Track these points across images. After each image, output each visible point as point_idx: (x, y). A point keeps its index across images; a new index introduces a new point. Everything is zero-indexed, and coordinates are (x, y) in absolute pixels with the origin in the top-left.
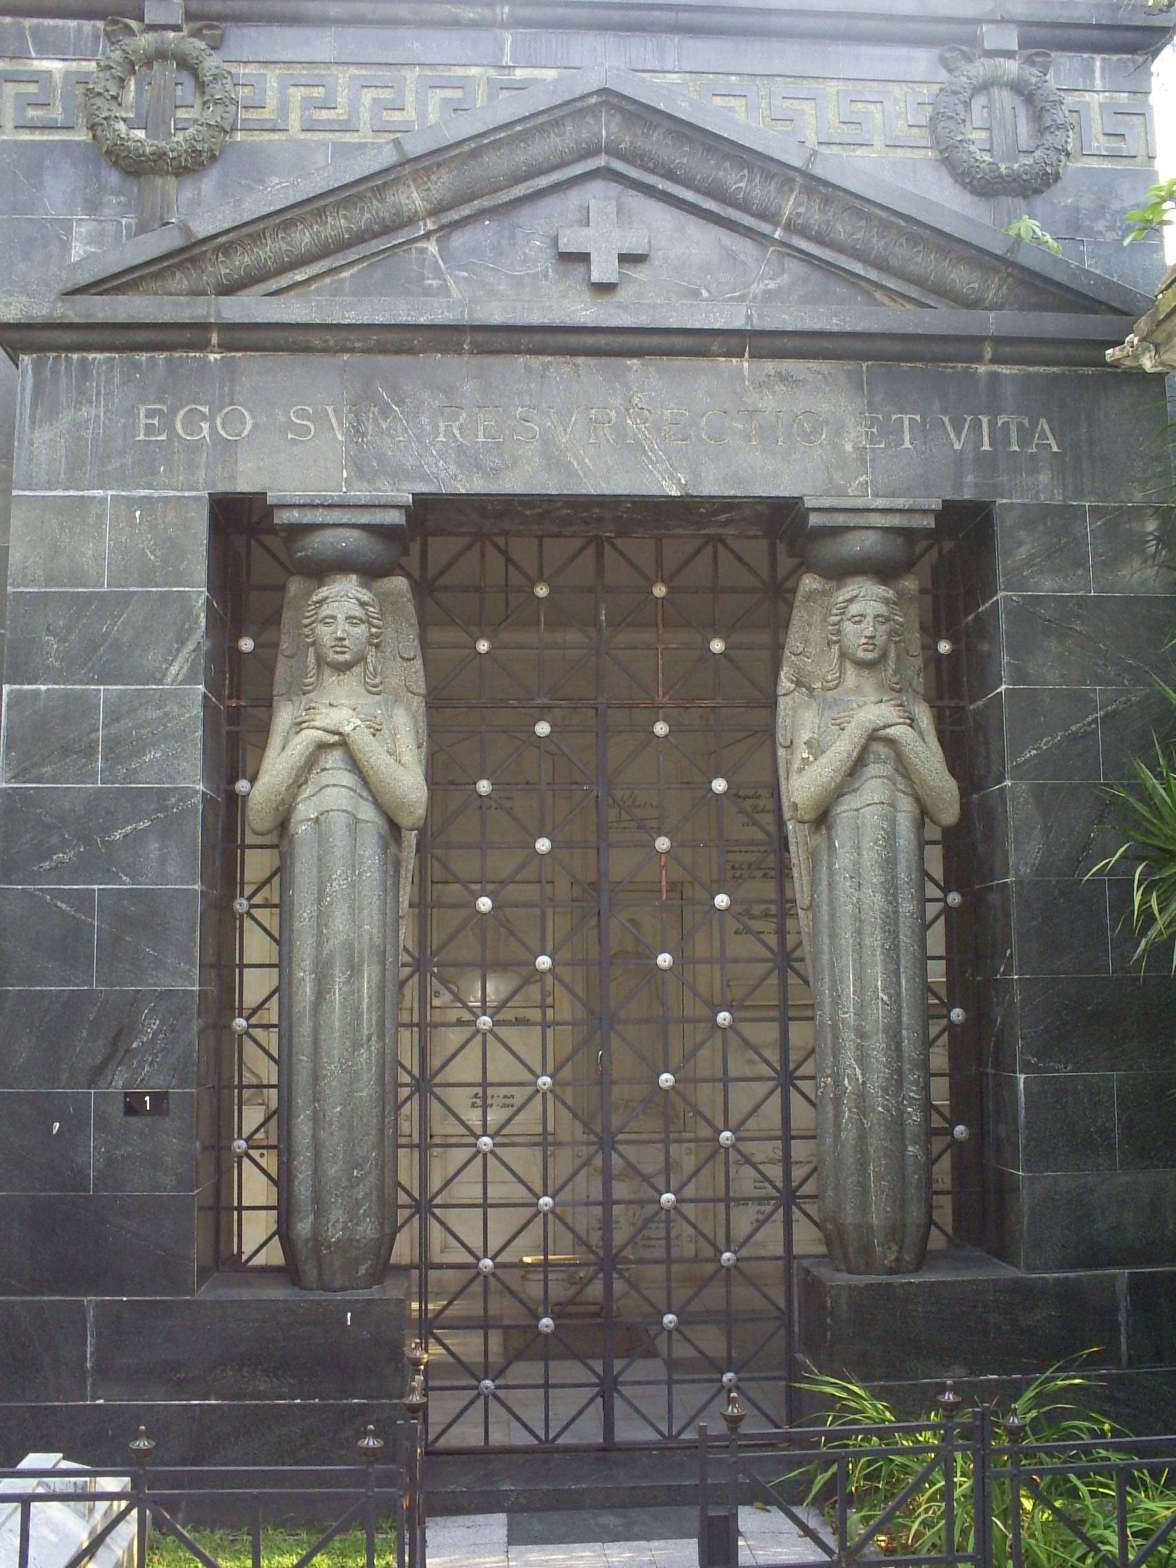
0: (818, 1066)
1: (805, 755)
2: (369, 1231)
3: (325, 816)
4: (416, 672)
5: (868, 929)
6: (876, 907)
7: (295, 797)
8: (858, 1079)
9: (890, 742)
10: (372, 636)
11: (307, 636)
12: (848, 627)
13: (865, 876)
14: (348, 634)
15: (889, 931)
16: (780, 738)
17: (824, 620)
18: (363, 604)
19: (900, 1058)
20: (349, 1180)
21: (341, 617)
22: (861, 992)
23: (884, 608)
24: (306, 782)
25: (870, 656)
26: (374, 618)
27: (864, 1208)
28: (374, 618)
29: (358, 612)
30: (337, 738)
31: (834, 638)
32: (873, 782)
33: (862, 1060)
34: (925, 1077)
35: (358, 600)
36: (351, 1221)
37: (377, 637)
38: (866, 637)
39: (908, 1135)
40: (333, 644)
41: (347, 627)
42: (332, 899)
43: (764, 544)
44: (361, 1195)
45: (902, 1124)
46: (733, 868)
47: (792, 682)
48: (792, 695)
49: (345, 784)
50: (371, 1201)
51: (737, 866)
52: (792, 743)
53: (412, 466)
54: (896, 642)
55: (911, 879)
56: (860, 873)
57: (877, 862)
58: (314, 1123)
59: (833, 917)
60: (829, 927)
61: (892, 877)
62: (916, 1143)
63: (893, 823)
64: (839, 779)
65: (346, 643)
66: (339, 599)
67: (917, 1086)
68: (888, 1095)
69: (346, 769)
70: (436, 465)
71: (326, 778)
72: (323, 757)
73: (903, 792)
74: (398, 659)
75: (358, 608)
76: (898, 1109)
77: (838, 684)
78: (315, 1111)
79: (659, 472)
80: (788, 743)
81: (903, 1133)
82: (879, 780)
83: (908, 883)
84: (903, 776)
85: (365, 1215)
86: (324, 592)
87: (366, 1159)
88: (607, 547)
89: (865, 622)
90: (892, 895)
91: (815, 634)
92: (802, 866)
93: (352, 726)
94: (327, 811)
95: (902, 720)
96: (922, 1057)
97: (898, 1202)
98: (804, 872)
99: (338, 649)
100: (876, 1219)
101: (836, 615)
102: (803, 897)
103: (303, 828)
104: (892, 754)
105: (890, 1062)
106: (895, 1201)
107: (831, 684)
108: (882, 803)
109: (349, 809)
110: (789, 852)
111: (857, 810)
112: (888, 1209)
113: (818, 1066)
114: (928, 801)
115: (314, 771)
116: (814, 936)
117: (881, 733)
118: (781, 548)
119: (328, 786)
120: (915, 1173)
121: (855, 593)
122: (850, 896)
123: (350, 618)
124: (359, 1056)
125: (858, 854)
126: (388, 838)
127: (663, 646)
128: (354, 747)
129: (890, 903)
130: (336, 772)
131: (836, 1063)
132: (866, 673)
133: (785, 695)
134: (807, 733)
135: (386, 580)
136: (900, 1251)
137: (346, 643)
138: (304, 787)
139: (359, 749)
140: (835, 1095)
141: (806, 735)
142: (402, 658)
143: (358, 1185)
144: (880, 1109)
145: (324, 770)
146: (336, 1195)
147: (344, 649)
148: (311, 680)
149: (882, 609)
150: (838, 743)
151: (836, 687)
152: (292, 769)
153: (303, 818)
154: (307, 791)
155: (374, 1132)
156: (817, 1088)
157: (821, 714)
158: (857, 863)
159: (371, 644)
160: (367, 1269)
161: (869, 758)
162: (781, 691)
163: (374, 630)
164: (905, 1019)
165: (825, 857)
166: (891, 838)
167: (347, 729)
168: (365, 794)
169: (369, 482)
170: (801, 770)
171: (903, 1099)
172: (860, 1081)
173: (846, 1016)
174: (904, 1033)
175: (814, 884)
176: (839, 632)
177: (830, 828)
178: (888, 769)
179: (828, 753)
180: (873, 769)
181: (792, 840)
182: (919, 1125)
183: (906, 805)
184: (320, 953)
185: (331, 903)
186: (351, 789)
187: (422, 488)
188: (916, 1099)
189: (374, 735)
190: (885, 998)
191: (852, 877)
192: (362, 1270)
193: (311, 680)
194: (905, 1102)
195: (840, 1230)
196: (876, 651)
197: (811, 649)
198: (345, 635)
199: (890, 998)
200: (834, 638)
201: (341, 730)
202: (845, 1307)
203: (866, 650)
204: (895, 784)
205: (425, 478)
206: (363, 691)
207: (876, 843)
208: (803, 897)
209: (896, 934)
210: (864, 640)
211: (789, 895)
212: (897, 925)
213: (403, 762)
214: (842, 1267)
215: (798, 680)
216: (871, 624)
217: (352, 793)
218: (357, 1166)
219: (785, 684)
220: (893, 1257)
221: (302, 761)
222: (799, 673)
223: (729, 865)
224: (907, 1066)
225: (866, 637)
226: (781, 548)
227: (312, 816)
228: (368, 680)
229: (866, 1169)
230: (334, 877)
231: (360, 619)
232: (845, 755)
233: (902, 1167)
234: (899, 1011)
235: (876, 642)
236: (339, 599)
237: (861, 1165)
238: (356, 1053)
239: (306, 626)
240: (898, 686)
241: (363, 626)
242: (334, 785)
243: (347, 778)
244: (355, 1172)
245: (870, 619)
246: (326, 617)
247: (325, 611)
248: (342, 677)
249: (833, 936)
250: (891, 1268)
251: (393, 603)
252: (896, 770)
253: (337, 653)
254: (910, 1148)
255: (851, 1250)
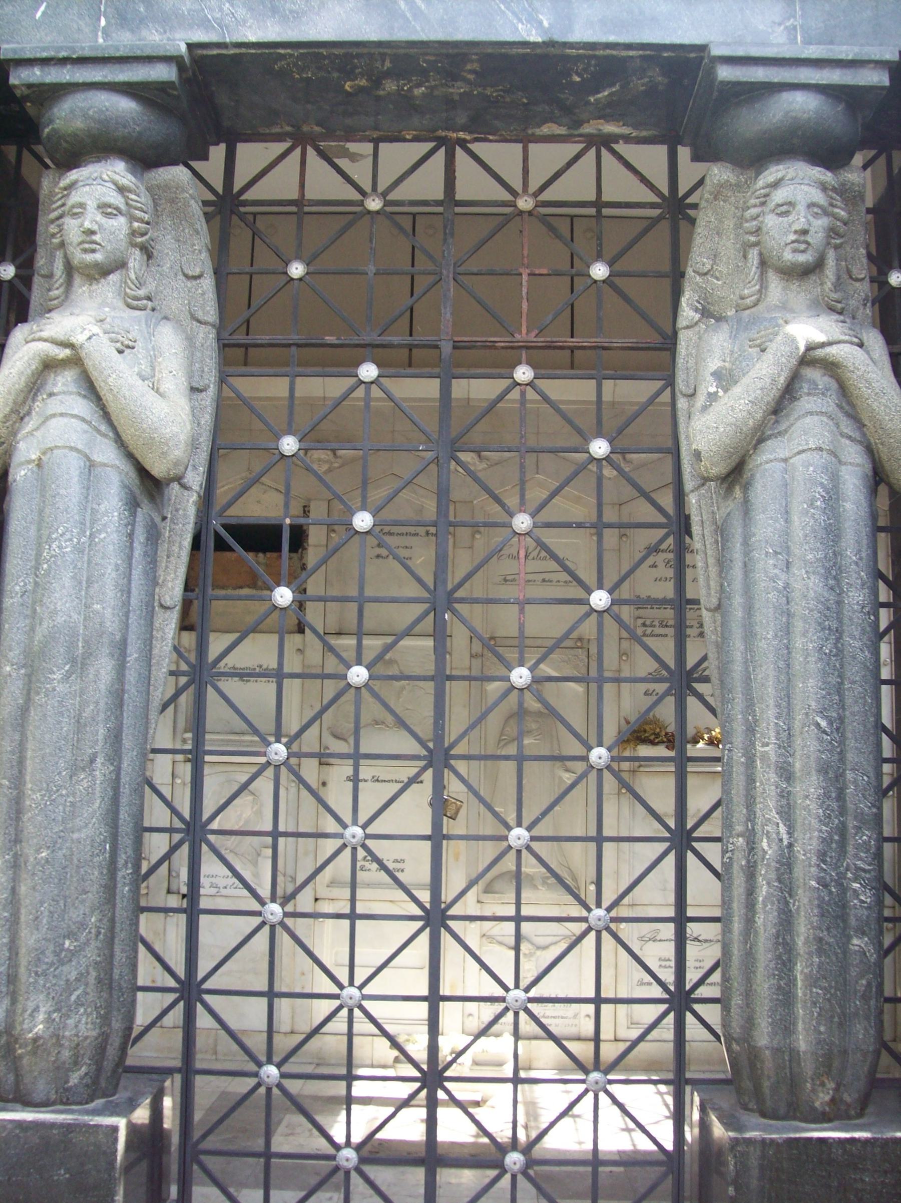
0: (727, 825)
1: (712, 389)
2: (82, 1026)
3: (48, 455)
4: (203, 294)
5: (799, 625)
6: (812, 594)
7: (14, 433)
8: (781, 840)
9: (831, 367)
10: (134, 233)
11: (53, 235)
12: (771, 221)
13: (797, 551)
14: (100, 226)
15: (829, 629)
16: (681, 384)
17: (739, 226)
18: (122, 190)
19: (843, 811)
20: (57, 954)
21: (91, 205)
22: (788, 714)
23: (821, 196)
24: (29, 413)
25: (801, 258)
26: (136, 208)
27: (786, 1026)
28: (136, 208)
29: (117, 200)
30: (67, 352)
31: (753, 239)
32: (808, 420)
33: (787, 813)
34: (877, 840)
35: (115, 183)
36: (58, 1010)
37: (143, 235)
38: (796, 232)
39: (853, 922)
40: (80, 240)
41: (99, 217)
42: (49, 566)
43: (662, 151)
44: (73, 976)
45: (844, 906)
46: (644, 625)
47: (696, 310)
48: (696, 329)
49: (75, 412)
50: (87, 984)
51: (648, 623)
52: (695, 390)
53: (189, 11)
54: (836, 247)
55: (861, 559)
56: (788, 548)
57: (814, 531)
58: (15, 873)
59: (749, 609)
60: (744, 626)
61: (834, 553)
62: (864, 933)
63: (835, 478)
64: (759, 415)
65: (97, 238)
66: (90, 182)
67: (868, 851)
68: (824, 862)
69: (79, 394)
70: (221, 10)
71: (54, 406)
72: (50, 382)
73: (849, 438)
74: (181, 277)
75: (115, 194)
76: (839, 884)
77: (758, 301)
78: (16, 856)
79: (513, 13)
80: (691, 391)
81: (843, 917)
82: (816, 418)
83: (856, 564)
84: (848, 415)
85: (79, 1003)
86: (73, 175)
87: (82, 925)
88: (459, 151)
89: (794, 214)
90: (835, 578)
91: (728, 246)
92: (709, 552)
93: (87, 334)
94: (51, 449)
95: (847, 338)
96: (874, 810)
97: (836, 1019)
98: (711, 561)
99: (87, 246)
100: (803, 1042)
101: (755, 206)
102: (709, 595)
103: (23, 473)
104: (834, 385)
105: (829, 817)
106: (832, 1017)
107: (748, 301)
108: (820, 449)
109: (80, 447)
110: (691, 537)
111: (785, 460)
112: (822, 1029)
113: (727, 825)
114: (884, 453)
115: (40, 398)
116: (722, 647)
117: (820, 353)
118: (684, 153)
119: (54, 416)
120: (862, 977)
121: (780, 175)
122: (773, 579)
123: (104, 208)
124: (78, 782)
125: (786, 521)
126: (137, 492)
127: (528, 271)
128: (89, 364)
129: (832, 589)
130: (67, 397)
131: (751, 817)
132: (795, 286)
133: (687, 327)
134: (716, 361)
135: (161, 170)
136: (837, 1090)
137: (97, 238)
138: (26, 419)
139: (94, 366)
140: (748, 862)
141: (714, 364)
142: (186, 276)
143: (70, 960)
144: (813, 883)
145: (51, 395)
146: (36, 973)
147: (94, 246)
148: (56, 292)
149: (818, 197)
150: (758, 366)
151: (755, 305)
152: (9, 393)
153: (23, 459)
154: (30, 424)
155: (95, 888)
156: (724, 852)
157: (733, 337)
158: (787, 533)
159: (134, 245)
160: (82, 1078)
161: (801, 388)
162: (681, 322)
163: (136, 225)
164: (851, 756)
165: (740, 530)
166: (833, 497)
167: (79, 338)
168: (103, 428)
169: (132, 31)
170: (705, 408)
171: (847, 870)
172: (785, 842)
173: (766, 749)
174: (849, 775)
175: (723, 564)
176: (758, 231)
177: (746, 487)
178: (829, 403)
179: (745, 381)
180: (806, 403)
181: (695, 519)
182: (869, 908)
183: (854, 455)
184: (31, 639)
185: (48, 573)
186: (83, 420)
187: (200, 36)
188: (864, 871)
189: (120, 352)
190: (823, 724)
191: (776, 553)
192: (74, 1079)
193: (56, 292)
194: (849, 875)
195: (754, 1055)
196: (810, 252)
197: (722, 268)
198: (95, 227)
199: (830, 723)
200: (753, 239)
201: (73, 340)
202: (755, 1172)
203: (795, 251)
204: (837, 425)
205: (205, 23)
206: (120, 304)
207: (811, 505)
208: (709, 595)
209: (839, 633)
210: (793, 237)
211: (689, 595)
212: (840, 621)
213: (161, 390)
214: (752, 1105)
215: (704, 307)
216: (803, 214)
217: (85, 427)
218: (70, 935)
219: (687, 313)
220: (827, 1098)
221: (23, 383)
222: (705, 299)
223: (640, 621)
224: (851, 823)
225: (796, 232)
226: (684, 153)
227: (34, 457)
228: (128, 290)
229: (791, 970)
230: (54, 536)
231: (117, 209)
232: (768, 381)
233: (844, 968)
234: (842, 742)
235: (809, 239)
236: (90, 182)
237: (784, 964)
238: (75, 778)
239: (52, 222)
240: (839, 306)
241: (122, 220)
242: (62, 415)
243: (81, 406)
244: (67, 943)
245: (801, 208)
246: (73, 207)
247: (75, 198)
248: (94, 287)
249: (749, 635)
250: (824, 1113)
251: (172, 201)
252: (840, 407)
253: (85, 251)
254: (855, 941)
255: (766, 1084)
